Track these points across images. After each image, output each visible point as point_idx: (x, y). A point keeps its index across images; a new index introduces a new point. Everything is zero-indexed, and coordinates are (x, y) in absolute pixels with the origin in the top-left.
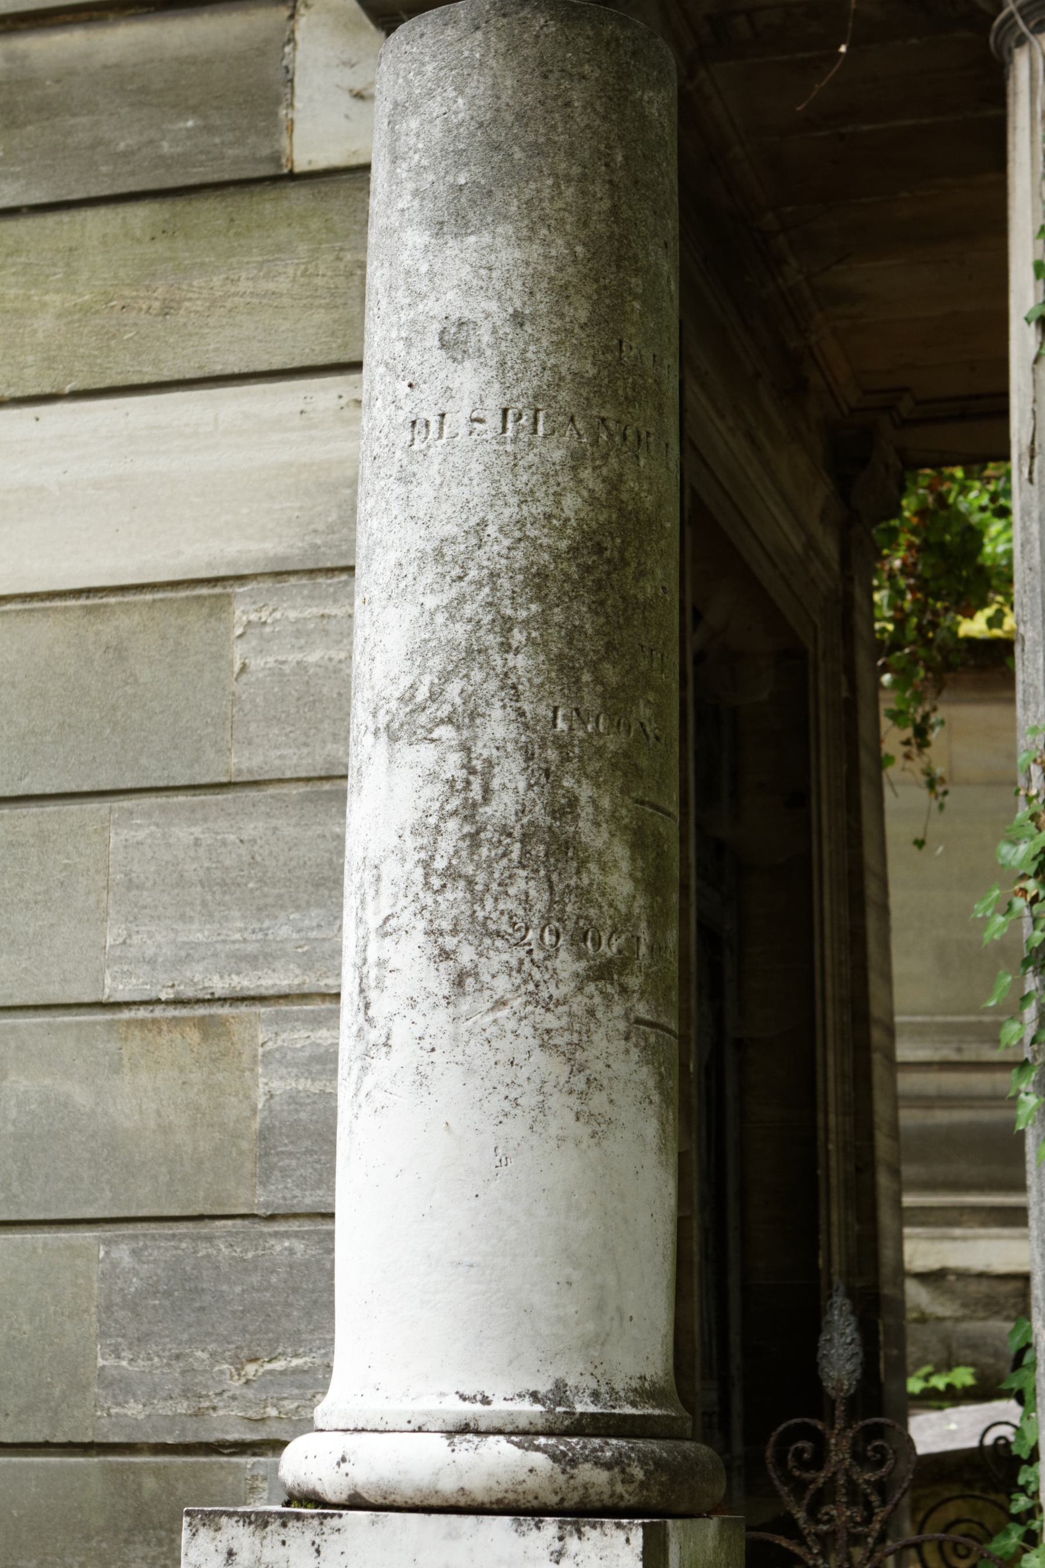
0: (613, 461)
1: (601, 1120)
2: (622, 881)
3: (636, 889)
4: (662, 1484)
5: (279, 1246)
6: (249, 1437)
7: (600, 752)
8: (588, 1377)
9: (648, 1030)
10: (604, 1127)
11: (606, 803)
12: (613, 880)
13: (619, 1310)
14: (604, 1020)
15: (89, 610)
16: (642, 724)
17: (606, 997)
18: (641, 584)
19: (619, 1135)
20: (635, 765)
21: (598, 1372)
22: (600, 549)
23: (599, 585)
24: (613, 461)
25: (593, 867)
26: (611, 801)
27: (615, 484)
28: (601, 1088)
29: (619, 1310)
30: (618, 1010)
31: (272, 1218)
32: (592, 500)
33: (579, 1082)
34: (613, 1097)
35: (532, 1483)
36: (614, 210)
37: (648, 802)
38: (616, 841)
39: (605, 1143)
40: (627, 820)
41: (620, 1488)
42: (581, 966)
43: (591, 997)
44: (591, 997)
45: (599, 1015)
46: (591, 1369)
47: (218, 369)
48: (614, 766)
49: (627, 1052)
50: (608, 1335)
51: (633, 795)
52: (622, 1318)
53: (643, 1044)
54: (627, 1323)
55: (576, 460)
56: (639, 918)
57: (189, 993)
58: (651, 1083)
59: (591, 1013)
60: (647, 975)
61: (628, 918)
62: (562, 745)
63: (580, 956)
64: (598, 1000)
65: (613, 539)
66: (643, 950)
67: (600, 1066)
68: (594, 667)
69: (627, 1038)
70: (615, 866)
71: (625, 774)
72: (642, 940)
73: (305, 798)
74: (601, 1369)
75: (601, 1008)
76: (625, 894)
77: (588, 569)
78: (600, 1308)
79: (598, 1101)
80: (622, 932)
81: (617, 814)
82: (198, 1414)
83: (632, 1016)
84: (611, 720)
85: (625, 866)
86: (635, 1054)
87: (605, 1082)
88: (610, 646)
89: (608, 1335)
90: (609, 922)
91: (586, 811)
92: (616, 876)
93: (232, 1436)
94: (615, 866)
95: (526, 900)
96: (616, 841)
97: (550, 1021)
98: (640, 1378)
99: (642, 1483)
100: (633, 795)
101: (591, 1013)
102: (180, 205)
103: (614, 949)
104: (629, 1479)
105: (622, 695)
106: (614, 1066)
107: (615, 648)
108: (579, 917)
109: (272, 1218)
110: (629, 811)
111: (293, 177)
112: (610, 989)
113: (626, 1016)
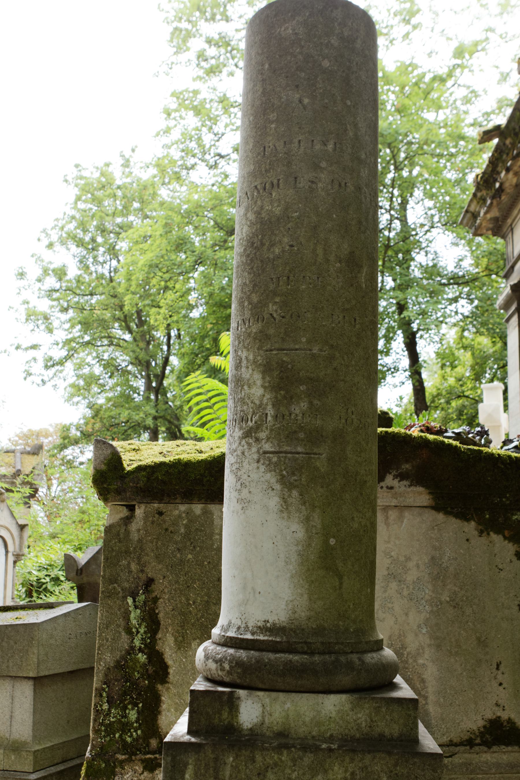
0: (259, 203)
1: (245, 501)
2: (257, 390)
3: (265, 391)
4: (238, 673)
8: (239, 619)
9: (271, 455)
10: (246, 504)
11: (251, 357)
12: (253, 391)
13: (253, 589)
14: (248, 456)
16: (271, 314)
17: (249, 444)
18: (272, 250)
19: (253, 507)
20: (266, 335)
21: (243, 618)
25: (246, 387)
26: (254, 355)
27: (258, 213)
28: (246, 487)
29: (253, 589)
30: (254, 449)
34: (251, 490)
37: (275, 349)
38: (255, 372)
39: (247, 511)
40: (261, 361)
41: (220, 673)
43: (243, 446)
44: (243, 446)
45: (246, 454)
46: (240, 616)
48: (255, 339)
49: (258, 468)
50: (248, 600)
51: (264, 348)
52: (254, 592)
53: (267, 463)
54: (257, 595)
55: (247, 210)
56: (267, 404)
58: (273, 480)
59: (243, 453)
60: (271, 430)
61: (260, 406)
63: (241, 428)
64: (246, 447)
65: (258, 237)
66: (269, 418)
67: (245, 477)
69: (258, 462)
70: (254, 384)
71: (260, 341)
72: (269, 415)
74: (244, 617)
75: (247, 450)
76: (259, 395)
77: (248, 256)
78: (245, 588)
80: (257, 413)
81: (95, 389)
83: (261, 451)
84: (254, 318)
85: (259, 383)
86: (262, 468)
87: (247, 484)
88: (255, 286)
89: (248, 600)
90: (251, 410)
92: (255, 388)
94: (254, 384)
96: (255, 372)
98: (265, 621)
99: (228, 671)
100: (264, 348)
101: (243, 453)
103: (253, 422)
104: (222, 669)
105: (260, 305)
106: (251, 476)
107: (257, 286)
108: (241, 411)
110: (262, 357)
112: (251, 441)
113: (258, 452)
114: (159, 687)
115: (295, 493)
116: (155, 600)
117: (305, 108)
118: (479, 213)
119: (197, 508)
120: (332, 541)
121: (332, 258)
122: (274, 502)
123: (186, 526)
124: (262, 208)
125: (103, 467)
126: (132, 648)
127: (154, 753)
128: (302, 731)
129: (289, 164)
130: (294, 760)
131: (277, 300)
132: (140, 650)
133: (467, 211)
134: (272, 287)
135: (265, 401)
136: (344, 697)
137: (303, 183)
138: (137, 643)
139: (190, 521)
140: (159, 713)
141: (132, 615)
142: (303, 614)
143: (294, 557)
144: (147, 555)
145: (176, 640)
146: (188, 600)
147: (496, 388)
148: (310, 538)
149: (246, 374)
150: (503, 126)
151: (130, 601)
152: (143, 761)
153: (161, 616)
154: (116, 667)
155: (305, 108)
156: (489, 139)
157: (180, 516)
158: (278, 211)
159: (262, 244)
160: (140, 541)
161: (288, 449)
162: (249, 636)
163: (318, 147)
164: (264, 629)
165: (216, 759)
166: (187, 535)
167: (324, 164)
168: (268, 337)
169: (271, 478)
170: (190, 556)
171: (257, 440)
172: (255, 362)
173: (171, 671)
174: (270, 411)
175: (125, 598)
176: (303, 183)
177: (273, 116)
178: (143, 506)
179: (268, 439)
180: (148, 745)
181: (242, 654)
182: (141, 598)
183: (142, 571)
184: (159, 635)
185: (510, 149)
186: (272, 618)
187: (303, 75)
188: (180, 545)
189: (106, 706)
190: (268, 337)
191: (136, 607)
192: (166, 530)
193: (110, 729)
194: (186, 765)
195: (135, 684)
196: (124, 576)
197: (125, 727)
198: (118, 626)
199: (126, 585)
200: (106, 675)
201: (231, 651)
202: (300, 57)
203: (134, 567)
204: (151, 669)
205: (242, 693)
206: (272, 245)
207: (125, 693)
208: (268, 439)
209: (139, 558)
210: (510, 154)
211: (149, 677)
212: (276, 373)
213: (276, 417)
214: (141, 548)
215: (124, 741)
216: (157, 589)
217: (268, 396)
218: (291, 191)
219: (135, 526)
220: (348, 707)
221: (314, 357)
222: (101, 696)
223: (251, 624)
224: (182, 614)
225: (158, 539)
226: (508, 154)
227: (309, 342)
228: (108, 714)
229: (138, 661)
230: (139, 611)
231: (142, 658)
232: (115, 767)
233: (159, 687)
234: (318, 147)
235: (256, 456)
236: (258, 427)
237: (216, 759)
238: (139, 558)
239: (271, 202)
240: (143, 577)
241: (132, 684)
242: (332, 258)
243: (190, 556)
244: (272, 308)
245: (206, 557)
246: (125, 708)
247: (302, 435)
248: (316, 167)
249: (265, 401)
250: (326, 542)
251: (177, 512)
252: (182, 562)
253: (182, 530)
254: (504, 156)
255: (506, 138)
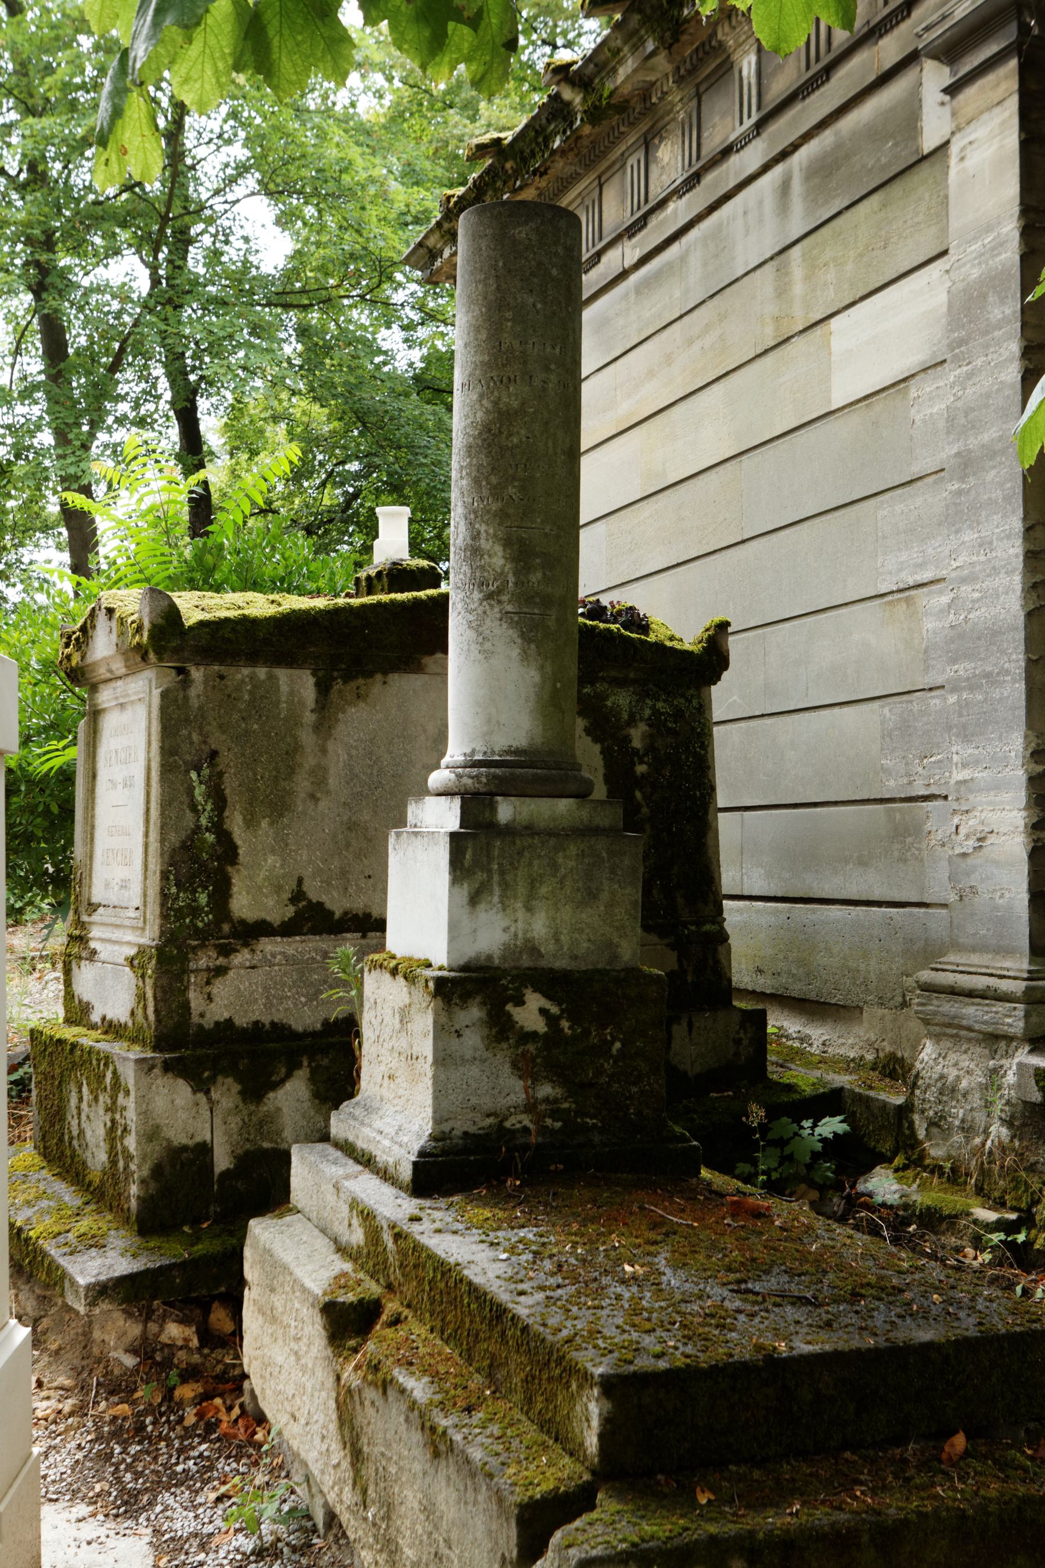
0: (496, 393)
5: (933, 702)
6: (926, 793)
7: (488, 512)
11: (491, 531)
12: (494, 560)
13: (498, 723)
15: (867, 406)
17: (491, 606)
22: (490, 430)
23: (489, 445)
24: (496, 393)
27: (495, 403)
30: (496, 610)
31: (931, 689)
32: (487, 412)
33: (480, 639)
35: (450, 784)
36: (498, 288)
42: (481, 596)
47: (902, 270)
48: (495, 516)
55: (481, 396)
57: (902, 586)
58: (515, 636)
61: (502, 573)
62: (475, 512)
63: (481, 591)
68: (487, 478)
73: (935, 482)
77: (485, 440)
78: (489, 721)
79: (488, 645)
82: (910, 783)
85: (500, 554)
86: (505, 626)
88: (493, 469)
91: (483, 535)
93: (921, 793)
95: (465, 574)
97: (471, 618)
102: (888, 189)
109: (931, 689)
111: (924, 158)
114: (229, 869)
115: (533, 646)
116: (221, 774)
117: (538, 312)
118: (441, 252)
119: (262, 672)
120: (559, 685)
121: (559, 451)
122: (515, 652)
123: (250, 692)
124: (499, 399)
125: (160, 621)
126: (198, 827)
127: (228, 938)
128: (543, 825)
129: (525, 362)
130: (542, 843)
131: (516, 484)
132: (207, 829)
133: (420, 245)
134: (511, 472)
135: (506, 569)
136: (572, 800)
137: (537, 382)
138: (204, 821)
139: (254, 687)
140: (231, 896)
141: (197, 792)
142: (539, 741)
143: (533, 697)
144: (209, 724)
145: (244, 819)
146: (255, 774)
147: (400, 514)
148: (544, 681)
149: (484, 544)
150: (506, 142)
151: (194, 775)
152: (216, 946)
153: (227, 792)
154: (181, 848)
155: (538, 312)
156: (483, 156)
157: (243, 681)
158: (515, 404)
159: (501, 433)
160: (200, 708)
161: (525, 610)
162: (497, 758)
163: (548, 350)
164: (508, 752)
165: (488, 844)
166: (252, 703)
167: (553, 367)
168: (508, 516)
169: (513, 633)
170: (256, 726)
171: (499, 602)
172: (495, 536)
173: (241, 851)
174: (511, 579)
175: (187, 772)
176: (537, 382)
177: (509, 315)
178: (202, 669)
179: (510, 602)
180: (220, 930)
181: (498, 771)
182: (206, 772)
183: (205, 742)
184: (227, 813)
185: (510, 176)
186: (515, 744)
187: (536, 280)
188: (244, 714)
189: (174, 890)
190: (508, 516)
191: (201, 783)
192: (229, 696)
193: (180, 915)
194: (466, 848)
195: (203, 865)
196: (185, 747)
197: (195, 911)
198: (182, 803)
199: (188, 758)
200: (172, 857)
201: (483, 769)
202: (533, 263)
203: (195, 737)
204: (220, 850)
205: (499, 798)
206: (510, 435)
207: (194, 876)
208: (510, 602)
209: (201, 728)
210: (511, 183)
211: (218, 859)
212: (516, 547)
213: (516, 584)
214: (202, 716)
215: (195, 926)
216: (222, 761)
217: (508, 566)
218: (527, 388)
219: (196, 690)
220: (575, 807)
221: (546, 535)
222: (168, 879)
223: (496, 749)
224: (250, 790)
225: (220, 706)
226: (505, 183)
227: (542, 522)
228: (177, 898)
229: (205, 840)
230: (203, 787)
231: (210, 837)
232: (187, 953)
233: (229, 869)
234: (548, 350)
235: (498, 616)
236: (499, 591)
237: (488, 844)
238: (201, 728)
239: (509, 396)
240: (206, 749)
241: (201, 866)
242: (559, 451)
243: (256, 726)
244: (511, 490)
245: (273, 728)
246: (195, 891)
247: (537, 600)
248: (547, 369)
249: (506, 569)
250: (555, 686)
251: (239, 676)
252: (247, 733)
253: (246, 697)
254: (499, 184)
255: (506, 160)
